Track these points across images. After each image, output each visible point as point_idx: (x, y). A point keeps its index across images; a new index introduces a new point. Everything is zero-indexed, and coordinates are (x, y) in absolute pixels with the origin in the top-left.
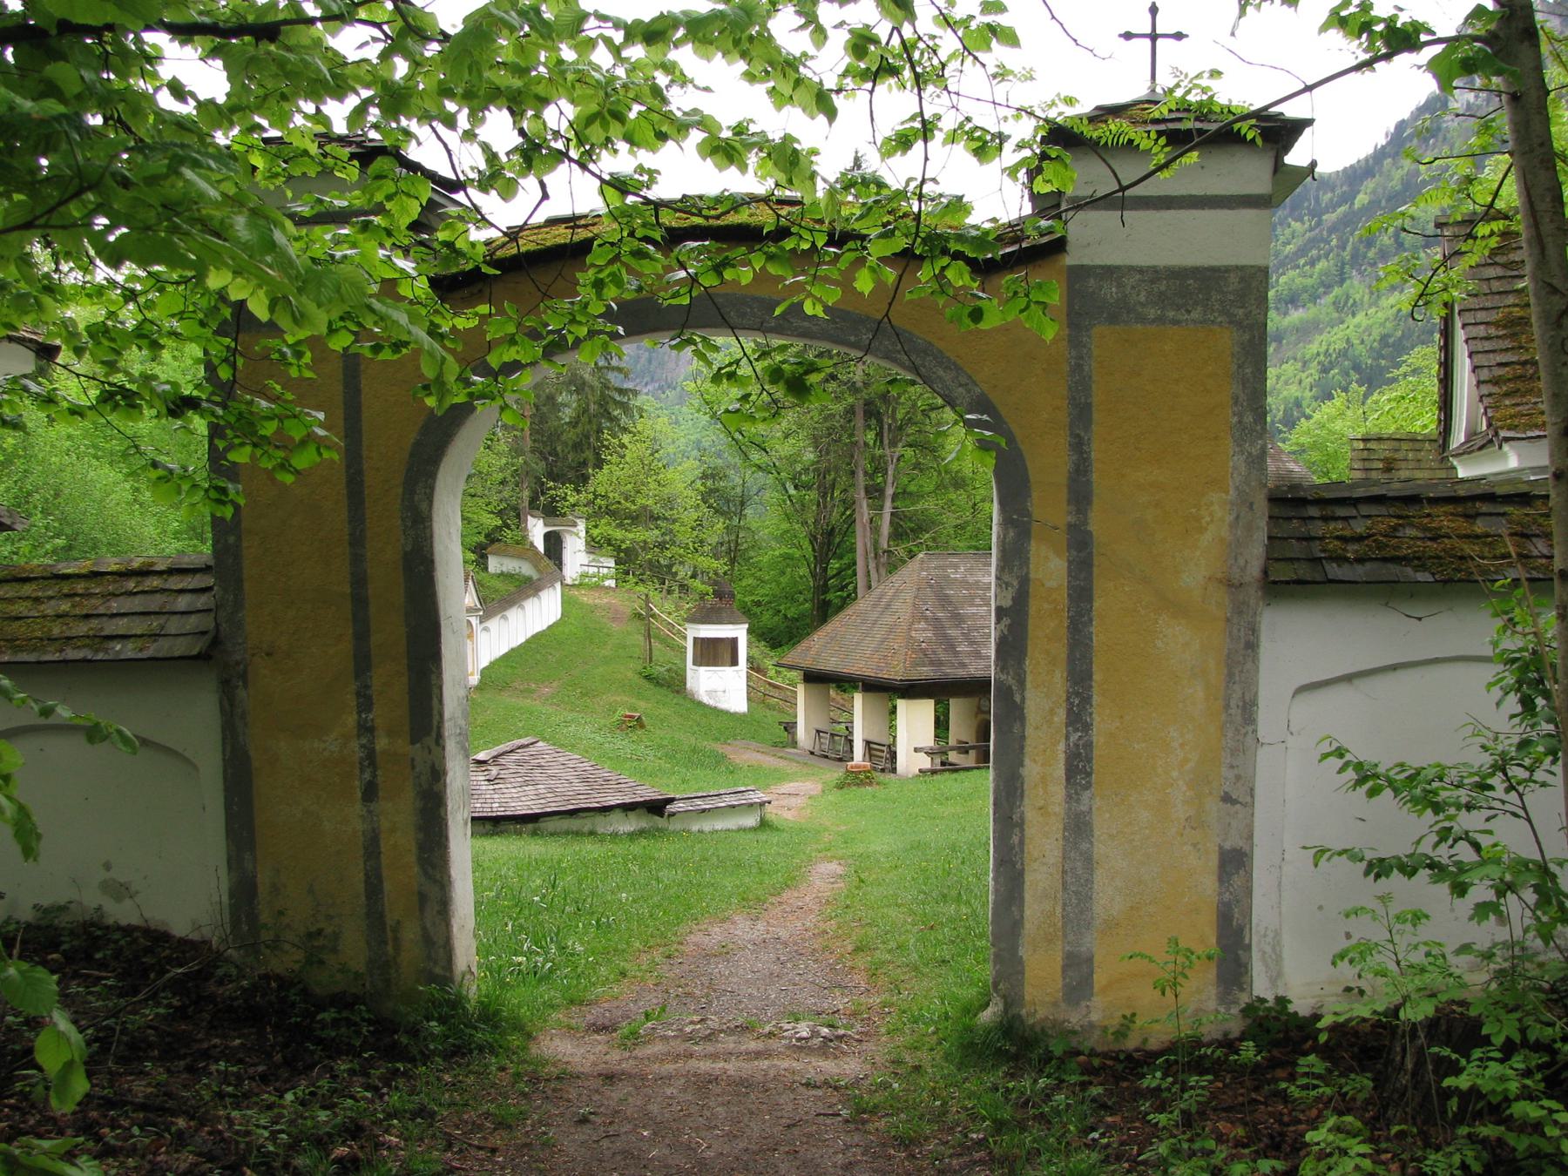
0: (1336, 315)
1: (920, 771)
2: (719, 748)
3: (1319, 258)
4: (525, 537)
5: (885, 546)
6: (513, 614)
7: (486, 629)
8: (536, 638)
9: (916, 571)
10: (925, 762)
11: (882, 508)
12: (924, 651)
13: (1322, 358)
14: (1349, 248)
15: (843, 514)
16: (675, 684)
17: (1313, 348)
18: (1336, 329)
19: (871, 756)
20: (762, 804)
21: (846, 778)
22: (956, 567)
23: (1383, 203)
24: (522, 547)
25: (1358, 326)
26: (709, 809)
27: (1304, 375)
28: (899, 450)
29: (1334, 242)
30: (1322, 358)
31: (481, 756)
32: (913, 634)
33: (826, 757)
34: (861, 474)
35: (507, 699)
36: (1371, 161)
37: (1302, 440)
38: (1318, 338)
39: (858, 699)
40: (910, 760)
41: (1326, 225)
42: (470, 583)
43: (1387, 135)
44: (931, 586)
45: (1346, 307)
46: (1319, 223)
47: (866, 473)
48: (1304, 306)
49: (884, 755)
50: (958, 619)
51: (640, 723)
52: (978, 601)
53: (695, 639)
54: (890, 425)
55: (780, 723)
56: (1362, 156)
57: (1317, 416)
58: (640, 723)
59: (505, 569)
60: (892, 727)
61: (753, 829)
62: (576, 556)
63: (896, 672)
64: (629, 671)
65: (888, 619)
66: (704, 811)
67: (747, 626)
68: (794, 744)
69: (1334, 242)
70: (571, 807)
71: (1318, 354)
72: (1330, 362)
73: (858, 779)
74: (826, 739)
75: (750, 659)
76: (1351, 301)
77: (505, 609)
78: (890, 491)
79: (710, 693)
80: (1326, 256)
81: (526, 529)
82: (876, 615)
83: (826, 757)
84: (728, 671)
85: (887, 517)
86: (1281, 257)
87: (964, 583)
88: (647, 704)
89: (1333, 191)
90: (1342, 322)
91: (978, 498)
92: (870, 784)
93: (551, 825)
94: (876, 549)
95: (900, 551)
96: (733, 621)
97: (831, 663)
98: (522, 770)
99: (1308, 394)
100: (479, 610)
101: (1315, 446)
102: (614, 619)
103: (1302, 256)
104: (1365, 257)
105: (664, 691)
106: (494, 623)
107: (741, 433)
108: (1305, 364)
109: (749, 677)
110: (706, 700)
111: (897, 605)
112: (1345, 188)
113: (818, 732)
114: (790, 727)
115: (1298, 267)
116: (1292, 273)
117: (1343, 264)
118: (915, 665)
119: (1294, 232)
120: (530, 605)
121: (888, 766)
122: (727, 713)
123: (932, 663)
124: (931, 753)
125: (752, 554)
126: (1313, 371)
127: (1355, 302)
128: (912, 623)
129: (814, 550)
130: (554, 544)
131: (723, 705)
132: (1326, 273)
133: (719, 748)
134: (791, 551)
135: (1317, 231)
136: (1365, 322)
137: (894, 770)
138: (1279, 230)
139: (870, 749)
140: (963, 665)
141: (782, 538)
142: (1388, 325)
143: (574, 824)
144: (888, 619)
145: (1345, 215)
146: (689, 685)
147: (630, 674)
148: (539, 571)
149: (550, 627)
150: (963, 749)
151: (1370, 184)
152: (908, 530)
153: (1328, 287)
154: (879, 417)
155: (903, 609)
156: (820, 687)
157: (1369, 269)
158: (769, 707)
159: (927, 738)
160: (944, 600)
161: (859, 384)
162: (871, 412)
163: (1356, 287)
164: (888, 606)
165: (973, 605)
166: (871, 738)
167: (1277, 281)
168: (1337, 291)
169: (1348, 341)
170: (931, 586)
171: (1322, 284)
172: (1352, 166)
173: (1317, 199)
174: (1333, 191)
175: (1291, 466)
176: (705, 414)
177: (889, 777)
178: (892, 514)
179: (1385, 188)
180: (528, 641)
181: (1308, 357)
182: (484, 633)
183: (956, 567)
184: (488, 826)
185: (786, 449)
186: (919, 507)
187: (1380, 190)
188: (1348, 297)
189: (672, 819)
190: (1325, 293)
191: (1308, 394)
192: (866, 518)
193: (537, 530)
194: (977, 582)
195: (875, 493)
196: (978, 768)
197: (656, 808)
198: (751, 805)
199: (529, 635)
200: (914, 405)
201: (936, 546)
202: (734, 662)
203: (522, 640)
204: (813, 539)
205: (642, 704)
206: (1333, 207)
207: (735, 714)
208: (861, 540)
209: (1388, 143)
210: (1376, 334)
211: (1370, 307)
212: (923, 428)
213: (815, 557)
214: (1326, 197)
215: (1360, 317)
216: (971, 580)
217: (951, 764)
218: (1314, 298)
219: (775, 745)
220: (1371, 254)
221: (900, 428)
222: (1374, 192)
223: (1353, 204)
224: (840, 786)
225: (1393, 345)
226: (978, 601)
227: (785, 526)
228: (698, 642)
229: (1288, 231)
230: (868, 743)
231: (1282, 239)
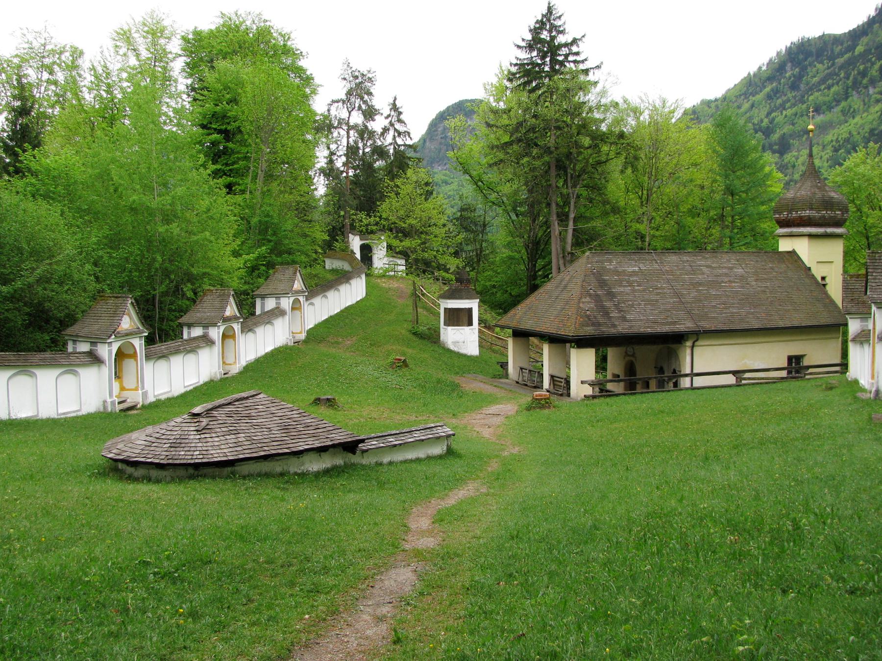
0: (843, 118)
1: (585, 396)
2: (457, 379)
3: (833, 85)
4: (348, 247)
5: (569, 250)
6: (331, 294)
7: (312, 304)
8: (348, 309)
9: (586, 261)
10: (589, 391)
11: (567, 226)
12: (588, 317)
13: (834, 143)
14: (851, 78)
15: (545, 231)
16: (432, 337)
17: (829, 138)
18: (843, 126)
19: (554, 385)
20: (448, 436)
21: (532, 404)
22: (610, 261)
23: (873, 51)
24: (347, 254)
25: (856, 124)
26: (400, 444)
27: (823, 154)
28: (578, 190)
29: (842, 75)
30: (834, 143)
31: (197, 410)
32: (581, 305)
33: (526, 385)
34: (554, 206)
35: (323, 348)
36: (866, 26)
37: (837, 179)
38: (832, 132)
39: (546, 348)
40: (579, 389)
41: (837, 66)
42: (298, 274)
43: (876, 9)
44: (594, 274)
45: (849, 113)
46: (833, 64)
47: (557, 205)
48: (824, 113)
49: (562, 385)
50: (611, 295)
51: (405, 364)
52: (624, 283)
53: (445, 309)
54: (572, 175)
55: (498, 363)
56: (861, 23)
57: (847, 164)
58: (405, 364)
59: (334, 267)
60: (568, 364)
61: (440, 457)
62: (380, 259)
63: (569, 330)
64: (403, 330)
65: (565, 296)
66: (395, 446)
67: (478, 300)
68: (506, 376)
69: (842, 75)
70: (262, 453)
71: (832, 141)
72: (839, 146)
73: (541, 404)
74: (526, 374)
75: (481, 321)
76: (852, 110)
77: (325, 291)
78: (572, 216)
79: (455, 343)
80: (837, 83)
81: (348, 242)
82: (556, 294)
83: (526, 385)
84: (466, 329)
85: (570, 232)
86: (811, 85)
87: (616, 272)
88: (413, 352)
89: (842, 44)
90: (846, 122)
91: (628, 220)
92: (549, 407)
93: (245, 469)
94: (564, 253)
95: (578, 252)
96: (469, 297)
97: (528, 325)
98: (230, 421)
99: (826, 164)
100: (304, 292)
101: (845, 183)
102: (400, 297)
103: (823, 84)
104: (861, 83)
105: (425, 342)
106: (317, 300)
107: (482, 182)
108: (824, 147)
109: (480, 331)
110: (452, 347)
111: (571, 285)
112: (849, 43)
113: (521, 369)
114: (504, 365)
115: (820, 90)
116: (816, 94)
117: (848, 88)
118: (583, 325)
119: (818, 70)
120: (344, 288)
121: (565, 392)
122: (465, 356)
123: (593, 324)
124: (592, 384)
125: (491, 256)
126: (828, 151)
127: (854, 111)
128: (581, 298)
129: (528, 254)
130: (366, 250)
131: (463, 351)
132: (836, 94)
133: (457, 379)
134: (513, 254)
135: (832, 69)
136: (861, 122)
137: (569, 395)
138: (809, 69)
139: (554, 381)
140: (614, 326)
141: (508, 245)
142: (874, 123)
143: (265, 467)
144: (565, 296)
145: (849, 59)
146: (441, 338)
147: (403, 331)
148: (352, 267)
149: (358, 302)
150: (616, 378)
151: (865, 40)
152: (583, 240)
153: (838, 102)
154: (565, 169)
155: (575, 290)
156: (523, 339)
157: (863, 91)
158: (494, 351)
159: (590, 374)
160: (602, 283)
161: (553, 149)
162: (561, 167)
163: (855, 101)
164: (566, 286)
165: (620, 286)
166: (554, 374)
167: (808, 99)
168: (843, 104)
169: (850, 133)
170: (594, 274)
171: (835, 100)
172: (854, 30)
173: (832, 51)
174: (842, 44)
175: (833, 194)
176: (460, 171)
177: (566, 400)
178: (574, 230)
179: (874, 42)
180: (342, 311)
181: (826, 143)
182: (310, 306)
183: (610, 261)
184: (191, 471)
185: (507, 189)
186: (590, 225)
187: (871, 43)
188: (850, 107)
189: (365, 454)
190: (836, 105)
191: (826, 164)
192: (557, 232)
193: (355, 243)
194: (624, 271)
195: (563, 218)
196: (624, 394)
197: (351, 447)
198: (438, 438)
199: (343, 307)
200: (587, 162)
201: (603, 248)
202: (470, 323)
203: (337, 311)
204: (527, 247)
205: (410, 351)
206: (841, 54)
207: (471, 356)
208: (555, 247)
209: (877, 15)
210: (867, 129)
211: (864, 112)
212: (593, 176)
213: (528, 258)
214: (837, 49)
215: (857, 119)
216: (620, 269)
217: (607, 391)
218: (830, 108)
219: (495, 377)
220: (865, 81)
221: (579, 176)
222: (867, 44)
223: (854, 52)
224: (529, 409)
225: (877, 135)
226: (624, 283)
227: (510, 239)
228: (448, 311)
229: (814, 70)
230: (552, 377)
231: (811, 74)
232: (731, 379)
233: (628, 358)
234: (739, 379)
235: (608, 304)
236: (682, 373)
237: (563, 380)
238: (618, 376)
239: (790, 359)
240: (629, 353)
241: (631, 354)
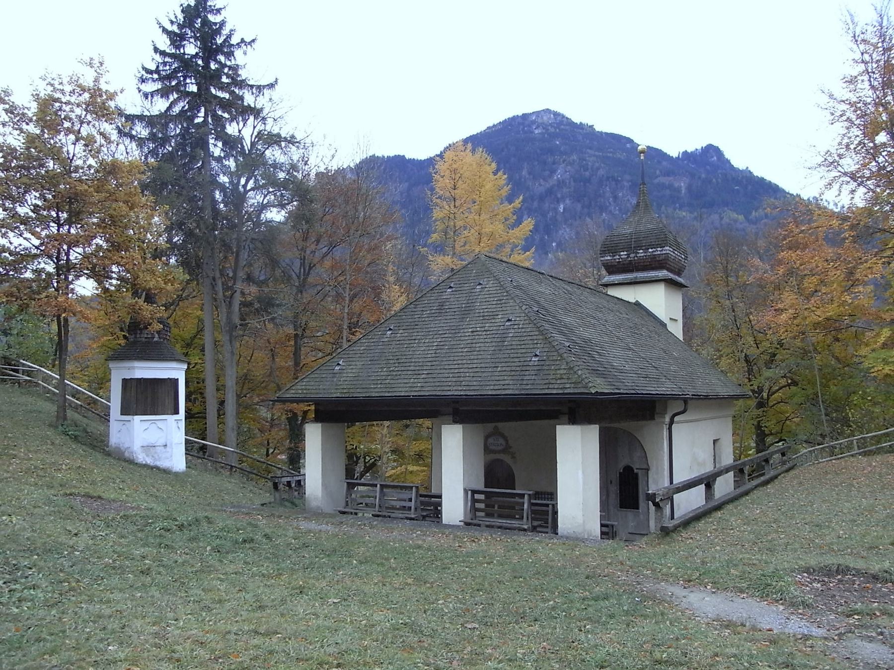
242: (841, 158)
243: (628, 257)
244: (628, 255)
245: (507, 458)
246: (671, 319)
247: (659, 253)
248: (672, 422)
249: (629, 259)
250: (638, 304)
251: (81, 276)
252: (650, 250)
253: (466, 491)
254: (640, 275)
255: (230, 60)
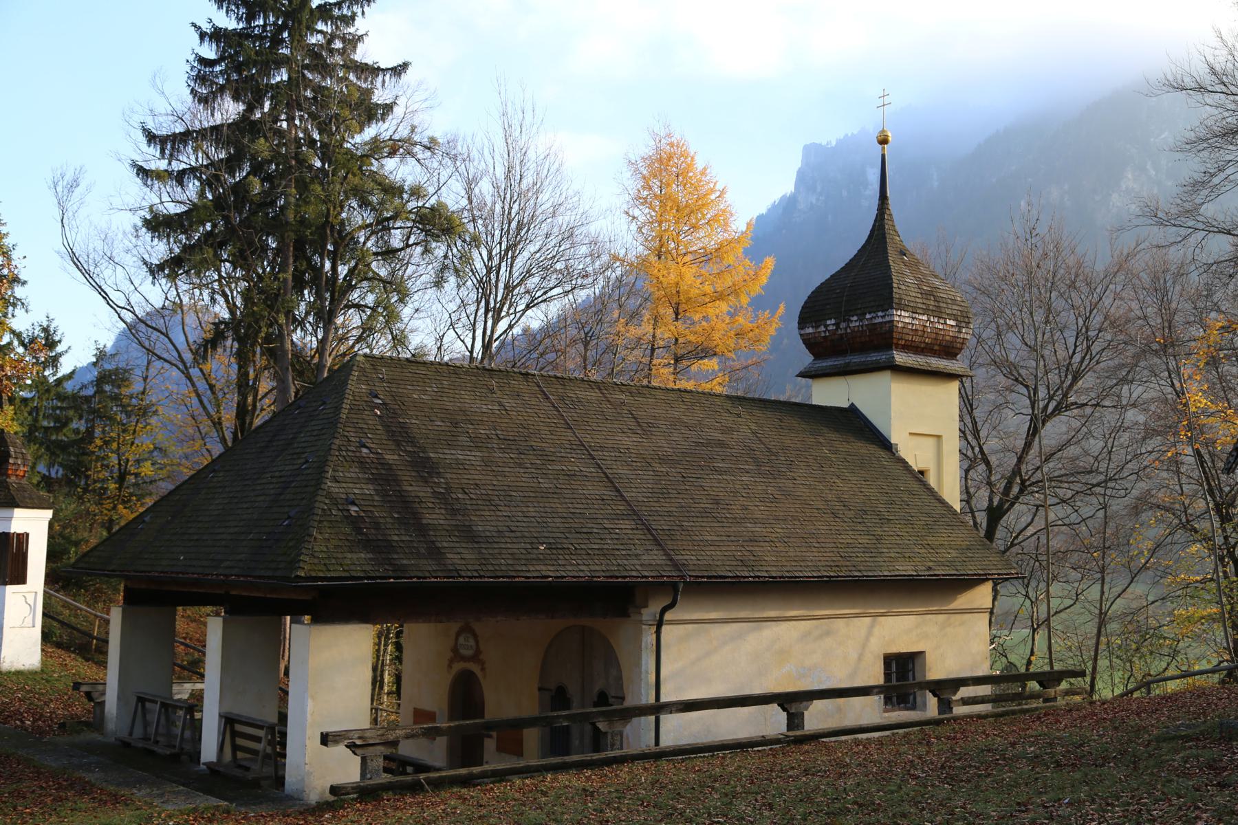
50: (425, 467)
113: (141, 700)
139: (235, 734)
230: (229, 722)
232: (773, 721)
233: (458, 666)
234: (795, 720)
235: (414, 489)
236: (629, 702)
237: (261, 733)
238: (431, 716)
239: (889, 660)
240: (464, 652)
241: (469, 653)
242: (119, 387)
243: (837, 329)
244: (837, 325)
245: (475, 668)
246: (910, 434)
247: (880, 320)
248: (659, 625)
249: (839, 332)
250: (853, 411)
251: (747, 228)
252: (868, 316)
253: (221, 716)
254: (856, 359)
255: (326, 24)
